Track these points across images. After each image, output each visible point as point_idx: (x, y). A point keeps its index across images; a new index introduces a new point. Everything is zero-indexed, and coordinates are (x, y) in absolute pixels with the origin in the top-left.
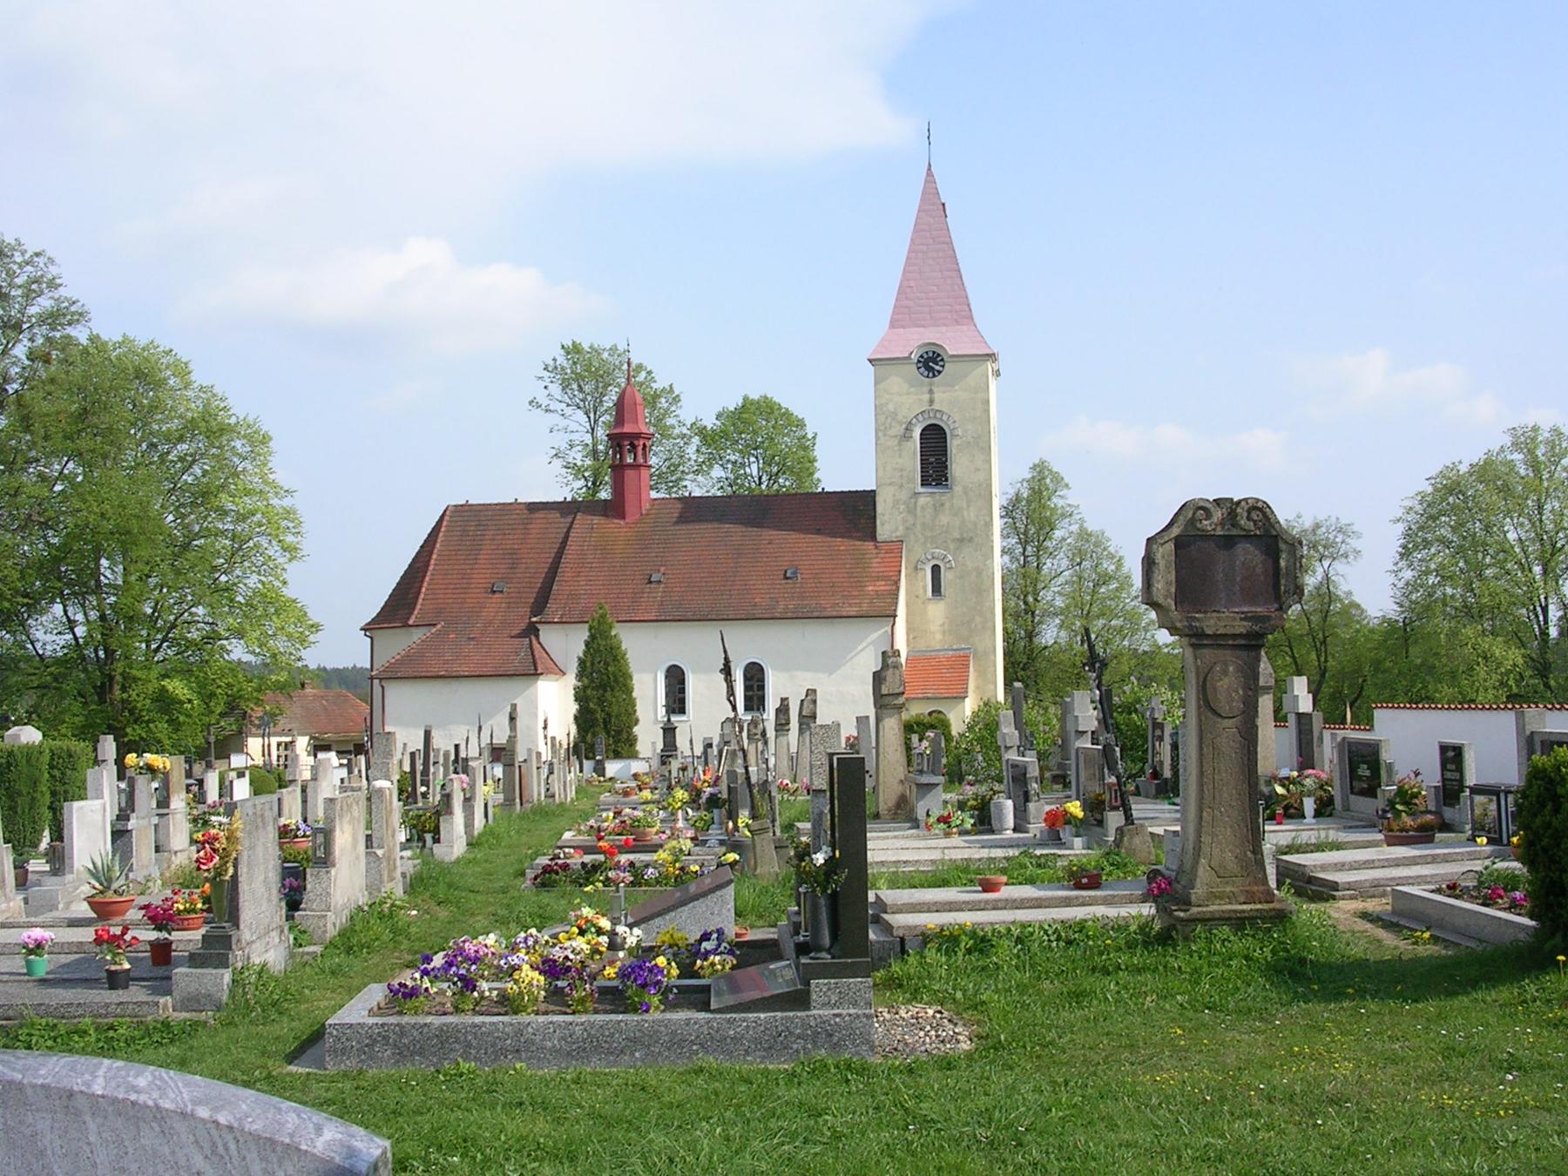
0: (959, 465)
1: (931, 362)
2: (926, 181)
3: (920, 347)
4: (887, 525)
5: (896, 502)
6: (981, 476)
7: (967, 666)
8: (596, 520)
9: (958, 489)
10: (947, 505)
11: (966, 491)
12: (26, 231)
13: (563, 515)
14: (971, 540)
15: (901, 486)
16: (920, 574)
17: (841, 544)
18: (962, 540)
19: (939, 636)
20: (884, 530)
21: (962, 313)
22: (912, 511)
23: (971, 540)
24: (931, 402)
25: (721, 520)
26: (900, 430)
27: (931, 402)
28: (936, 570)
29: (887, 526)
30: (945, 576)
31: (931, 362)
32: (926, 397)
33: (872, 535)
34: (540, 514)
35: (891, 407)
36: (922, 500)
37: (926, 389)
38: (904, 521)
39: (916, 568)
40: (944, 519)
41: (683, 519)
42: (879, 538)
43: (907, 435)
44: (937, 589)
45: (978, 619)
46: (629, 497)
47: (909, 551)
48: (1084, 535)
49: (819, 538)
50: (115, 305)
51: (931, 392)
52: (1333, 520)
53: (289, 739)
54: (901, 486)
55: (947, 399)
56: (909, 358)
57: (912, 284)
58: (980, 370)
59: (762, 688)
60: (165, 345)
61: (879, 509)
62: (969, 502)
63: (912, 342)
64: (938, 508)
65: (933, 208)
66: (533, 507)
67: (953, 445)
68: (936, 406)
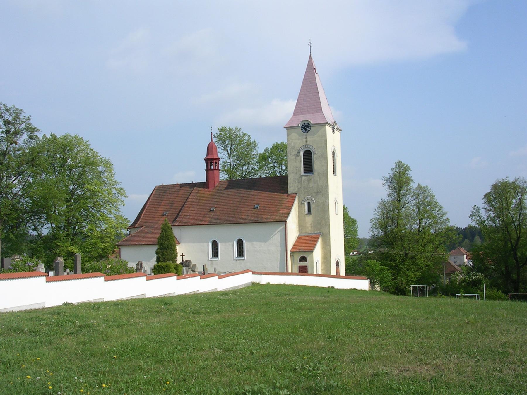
0: (316, 165)
1: (306, 127)
2: (309, 61)
3: (302, 121)
4: (292, 187)
5: (295, 179)
6: (324, 168)
7: (317, 240)
8: (200, 189)
9: (316, 173)
10: (312, 179)
11: (319, 174)
12: (11, 100)
13: (191, 188)
14: (321, 192)
15: (296, 173)
16: (303, 205)
17: (276, 195)
18: (318, 192)
19: (310, 228)
20: (291, 190)
21: (319, 109)
22: (300, 182)
23: (321, 192)
24: (306, 142)
25: (239, 188)
26: (295, 153)
27: (306, 142)
28: (309, 204)
29: (291, 188)
30: (312, 206)
31: (306, 127)
32: (305, 140)
33: (286, 191)
34: (183, 188)
35: (292, 144)
36: (304, 178)
37: (304, 137)
38: (298, 186)
39: (302, 203)
40: (311, 185)
41: (227, 188)
42: (289, 193)
43: (298, 155)
44: (309, 211)
45: (324, 222)
46: (211, 182)
47: (299, 197)
48: (419, 187)
49: (269, 193)
50: (49, 122)
51: (306, 138)
52: (522, 178)
53: (160, 264)
54: (296, 173)
55: (312, 140)
56: (298, 126)
57: (302, 99)
58: (323, 129)
59: (243, 248)
60: (72, 134)
61: (289, 182)
62: (320, 178)
63: (299, 122)
64: (309, 181)
65: (311, 70)
66: (182, 185)
67: (314, 157)
68: (308, 143)
